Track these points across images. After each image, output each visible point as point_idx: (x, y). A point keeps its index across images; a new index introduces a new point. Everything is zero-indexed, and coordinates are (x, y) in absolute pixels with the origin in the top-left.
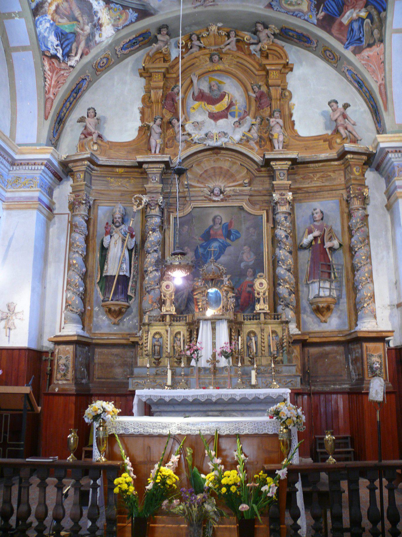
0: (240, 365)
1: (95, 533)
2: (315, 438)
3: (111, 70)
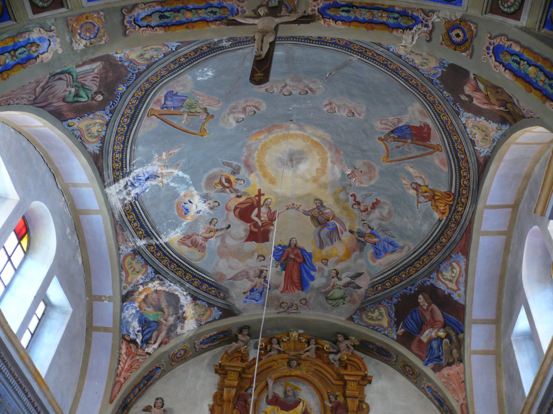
3: (187, 362)
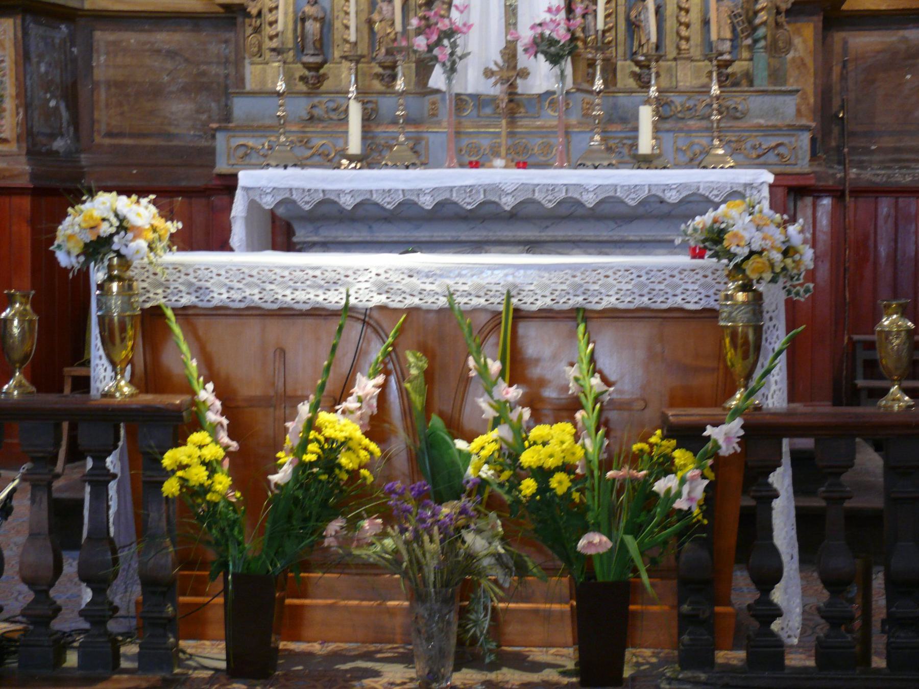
0: (598, 84)
1: (104, 623)
2: (853, 344)
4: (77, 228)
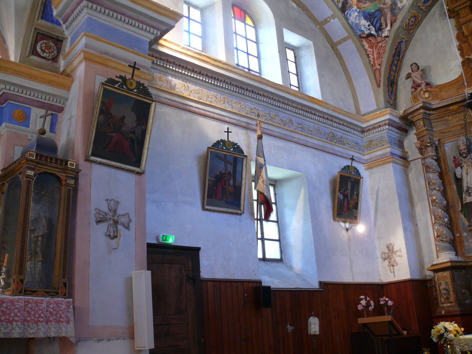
4: (435, 332)
